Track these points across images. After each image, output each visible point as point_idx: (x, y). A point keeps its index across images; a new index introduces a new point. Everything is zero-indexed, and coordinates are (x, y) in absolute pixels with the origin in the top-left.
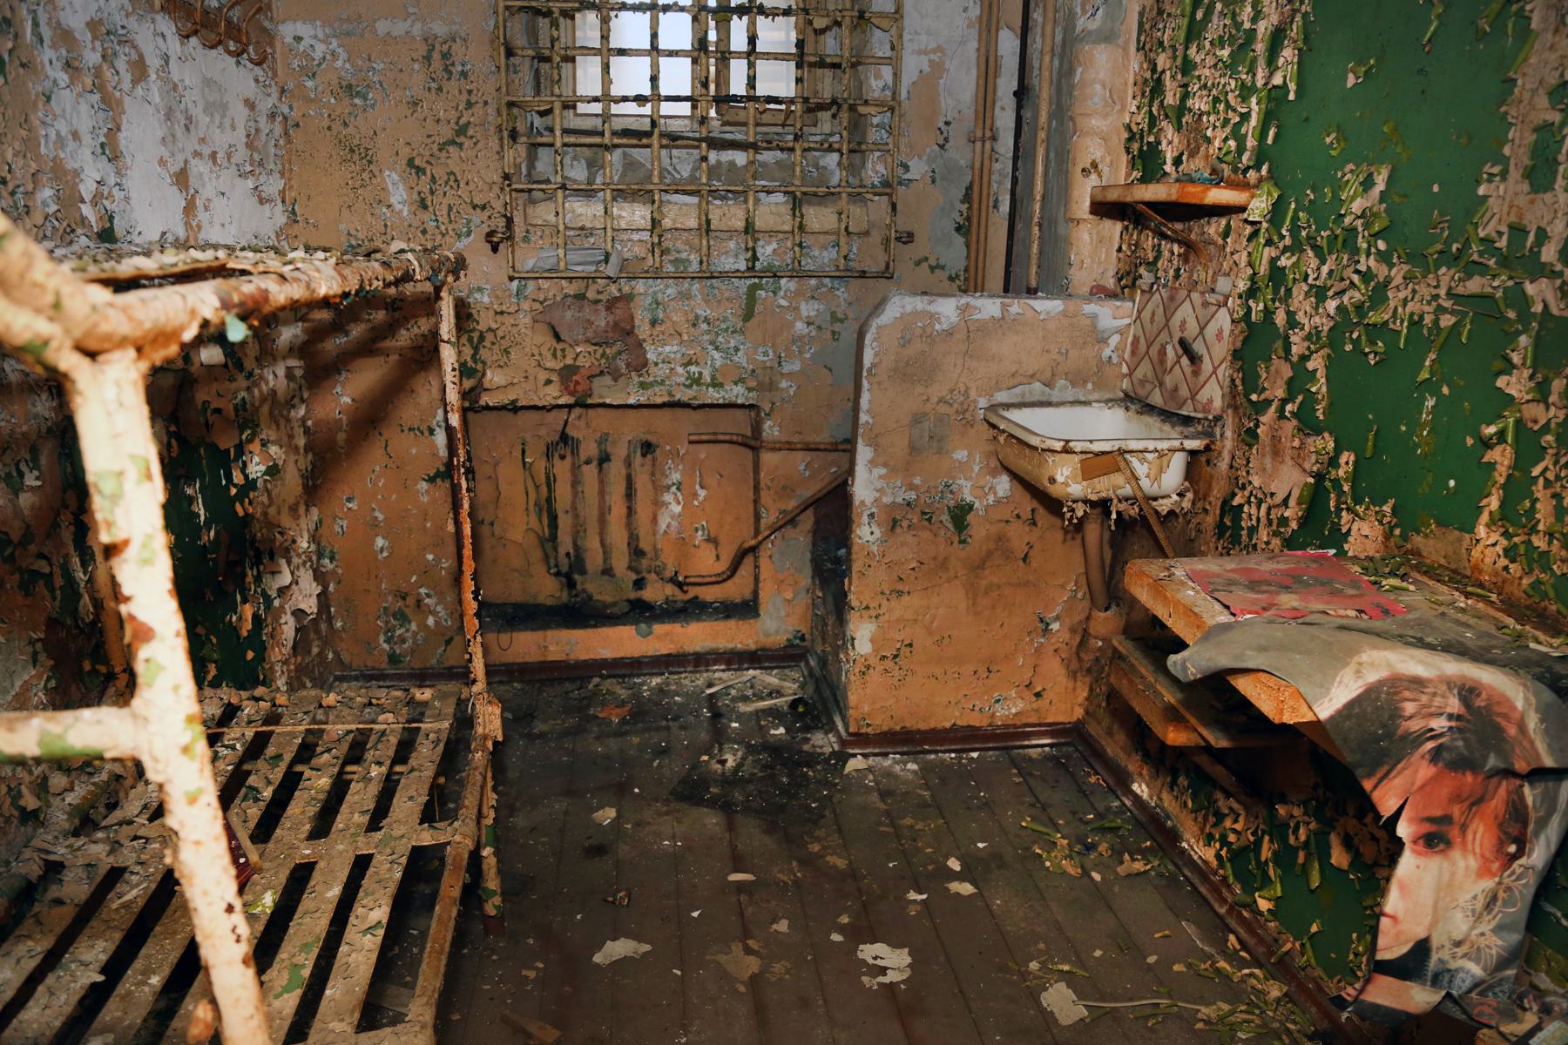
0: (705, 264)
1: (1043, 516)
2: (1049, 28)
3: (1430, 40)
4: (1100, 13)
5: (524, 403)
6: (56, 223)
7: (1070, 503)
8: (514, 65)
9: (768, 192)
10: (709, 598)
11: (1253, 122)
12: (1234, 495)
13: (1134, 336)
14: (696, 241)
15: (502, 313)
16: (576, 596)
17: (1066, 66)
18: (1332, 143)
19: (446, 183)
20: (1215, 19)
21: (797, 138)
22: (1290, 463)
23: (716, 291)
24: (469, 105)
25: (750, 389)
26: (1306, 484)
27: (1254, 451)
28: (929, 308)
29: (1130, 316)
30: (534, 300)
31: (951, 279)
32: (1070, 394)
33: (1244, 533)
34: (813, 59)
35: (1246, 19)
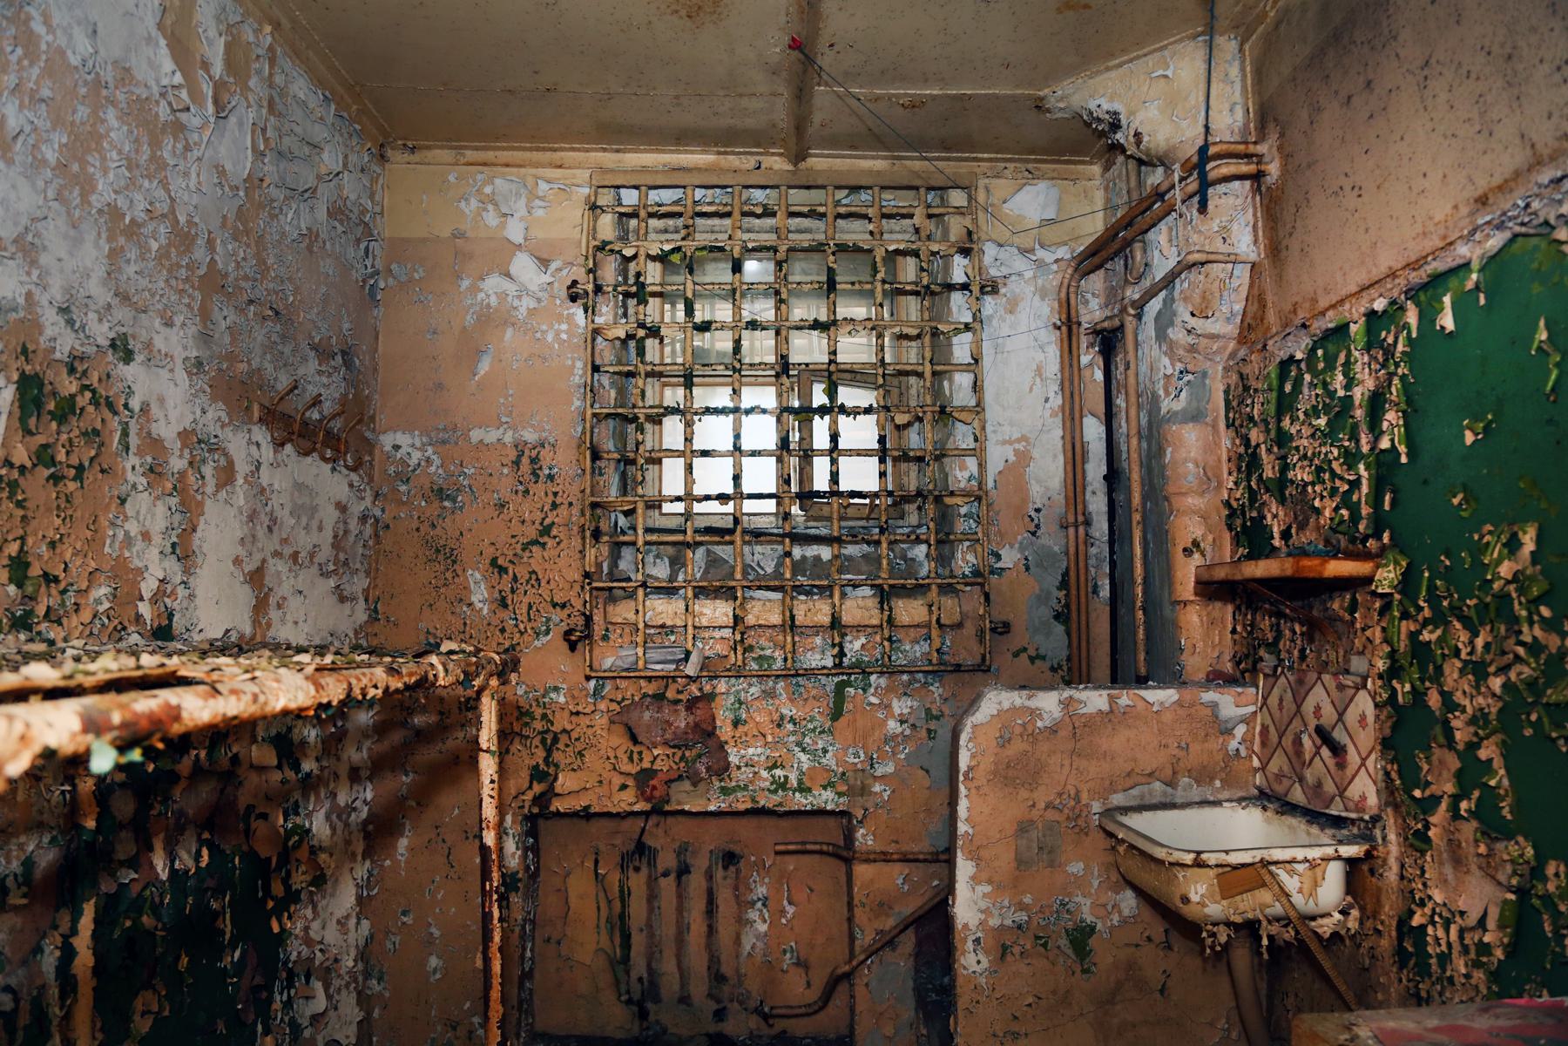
0: (790, 661)
1: (1178, 942)
2: (1133, 412)
3: (1553, 389)
4: (1183, 394)
5: (597, 810)
6: (106, 621)
7: (1210, 927)
8: (600, 468)
9: (855, 586)
10: (799, 1033)
11: (1365, 489)
12: (1412, 913)
13: (1263, 725)
14: (781, 638)
15: (578, 713)
16: (648, 1028)
17: (1154, 448)
18: (1460, 504)
19: (528, 582)
20: (1306, 390)
21: (882, 531)
22: (1478, 873)
23: (802, 690)
24: (554, 506)
25: (840, 794)
26: (1505, 902)
27: (1428, 858)
28: (1028, 703)
29: (1255, 703)
30: (611, 700)
31: (1053, 669)
32: (1196, 793)
33: (1433, 961)
34: (896, 453)
35: (1338, 387)
